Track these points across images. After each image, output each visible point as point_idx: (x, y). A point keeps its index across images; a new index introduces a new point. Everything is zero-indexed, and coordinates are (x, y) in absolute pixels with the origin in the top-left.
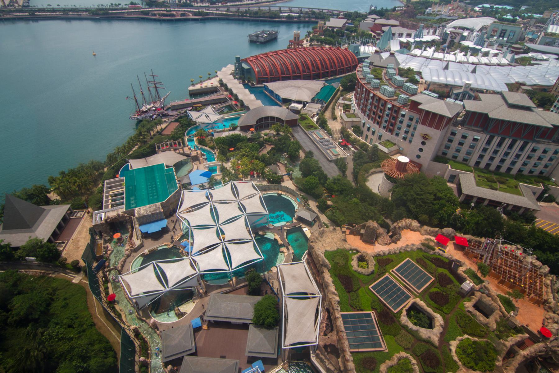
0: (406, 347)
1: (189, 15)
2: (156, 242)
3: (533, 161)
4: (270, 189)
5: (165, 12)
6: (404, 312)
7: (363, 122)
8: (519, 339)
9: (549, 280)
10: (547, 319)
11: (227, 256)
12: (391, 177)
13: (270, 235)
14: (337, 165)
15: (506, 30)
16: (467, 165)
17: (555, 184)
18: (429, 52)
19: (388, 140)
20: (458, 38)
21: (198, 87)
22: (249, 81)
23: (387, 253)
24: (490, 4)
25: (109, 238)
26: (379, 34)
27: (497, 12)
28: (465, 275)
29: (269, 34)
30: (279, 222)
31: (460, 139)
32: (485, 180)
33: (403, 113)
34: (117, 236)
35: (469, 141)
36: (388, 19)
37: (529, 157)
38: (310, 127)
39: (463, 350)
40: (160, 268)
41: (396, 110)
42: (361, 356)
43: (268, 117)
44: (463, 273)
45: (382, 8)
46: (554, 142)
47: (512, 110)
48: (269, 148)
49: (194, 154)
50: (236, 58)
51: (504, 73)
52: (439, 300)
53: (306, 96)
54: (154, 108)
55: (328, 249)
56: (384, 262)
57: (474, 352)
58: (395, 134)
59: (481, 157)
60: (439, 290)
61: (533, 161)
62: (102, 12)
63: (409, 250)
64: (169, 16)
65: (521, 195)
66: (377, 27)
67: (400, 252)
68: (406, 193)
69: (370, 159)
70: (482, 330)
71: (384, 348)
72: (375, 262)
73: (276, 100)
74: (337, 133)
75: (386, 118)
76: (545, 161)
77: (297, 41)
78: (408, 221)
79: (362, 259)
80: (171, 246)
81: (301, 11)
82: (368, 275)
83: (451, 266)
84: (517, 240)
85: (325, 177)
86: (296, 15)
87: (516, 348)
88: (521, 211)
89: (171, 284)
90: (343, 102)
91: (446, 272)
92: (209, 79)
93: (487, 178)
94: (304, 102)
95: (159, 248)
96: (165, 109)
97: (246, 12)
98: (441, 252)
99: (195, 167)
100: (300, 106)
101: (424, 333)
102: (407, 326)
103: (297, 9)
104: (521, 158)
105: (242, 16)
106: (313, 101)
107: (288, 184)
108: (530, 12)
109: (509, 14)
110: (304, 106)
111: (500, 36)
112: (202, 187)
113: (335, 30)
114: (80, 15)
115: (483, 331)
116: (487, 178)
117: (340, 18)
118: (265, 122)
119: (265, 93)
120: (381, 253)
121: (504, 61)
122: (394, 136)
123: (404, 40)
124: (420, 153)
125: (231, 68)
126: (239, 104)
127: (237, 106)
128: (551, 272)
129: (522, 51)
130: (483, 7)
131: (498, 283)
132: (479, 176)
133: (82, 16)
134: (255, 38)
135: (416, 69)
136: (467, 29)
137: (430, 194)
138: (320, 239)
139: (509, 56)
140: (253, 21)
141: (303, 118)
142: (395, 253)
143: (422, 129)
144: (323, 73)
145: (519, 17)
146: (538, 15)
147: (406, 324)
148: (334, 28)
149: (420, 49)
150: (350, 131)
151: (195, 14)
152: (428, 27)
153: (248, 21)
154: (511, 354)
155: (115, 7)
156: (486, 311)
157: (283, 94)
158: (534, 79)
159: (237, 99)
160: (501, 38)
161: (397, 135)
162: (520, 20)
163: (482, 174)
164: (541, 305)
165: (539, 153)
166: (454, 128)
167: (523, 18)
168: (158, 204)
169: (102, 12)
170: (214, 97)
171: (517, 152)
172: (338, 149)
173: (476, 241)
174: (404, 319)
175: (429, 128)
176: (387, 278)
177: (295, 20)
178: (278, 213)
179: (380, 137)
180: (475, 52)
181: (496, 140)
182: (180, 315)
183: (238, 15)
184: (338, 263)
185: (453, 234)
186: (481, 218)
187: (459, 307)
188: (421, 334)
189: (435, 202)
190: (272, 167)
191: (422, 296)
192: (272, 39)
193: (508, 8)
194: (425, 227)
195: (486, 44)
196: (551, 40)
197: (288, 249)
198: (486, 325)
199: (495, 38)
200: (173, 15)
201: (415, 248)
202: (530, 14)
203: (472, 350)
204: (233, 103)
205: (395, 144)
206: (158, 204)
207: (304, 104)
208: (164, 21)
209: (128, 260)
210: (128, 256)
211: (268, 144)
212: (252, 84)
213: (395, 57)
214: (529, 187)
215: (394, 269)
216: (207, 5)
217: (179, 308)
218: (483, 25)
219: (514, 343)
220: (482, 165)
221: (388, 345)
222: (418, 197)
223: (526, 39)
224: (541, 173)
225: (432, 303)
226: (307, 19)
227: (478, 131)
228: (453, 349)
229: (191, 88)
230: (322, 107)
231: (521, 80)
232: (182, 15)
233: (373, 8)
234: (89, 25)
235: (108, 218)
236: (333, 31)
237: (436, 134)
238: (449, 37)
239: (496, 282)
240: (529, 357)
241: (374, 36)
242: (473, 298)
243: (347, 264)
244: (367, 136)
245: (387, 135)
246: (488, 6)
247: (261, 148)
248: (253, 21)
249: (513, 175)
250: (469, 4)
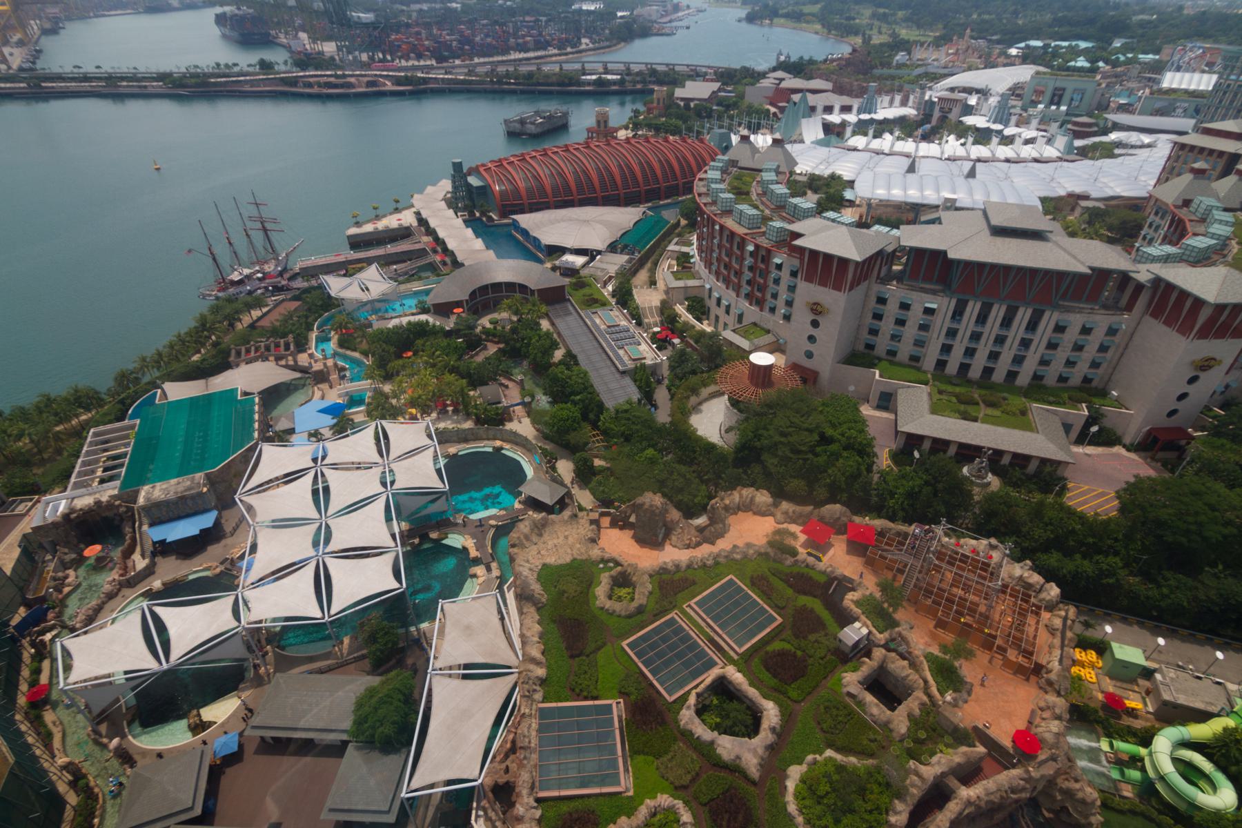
0: (677, 784)
1: (385, 85)
2: (187, 562)
3: (1062, 355)
4: (477, 438)
5: (332, 79)
6: (692, 700)
7: (708, 286)
8: (958, 759)
9: (1060, 616)
10: (1042, 709)
11: (323, 585)
12: (738, 402)
13: (455, 540)
14: (635, 381)
15: (1064, 89)
16: (919, 369)
17: (1119, 403)
18: (886, 142)
19: (755, 324)
20: (956, 110)
21: (368, 228)
22: (483, 213)
23: (684, 565)
25: (74, 556)
26: (782, 110)
27: (1056, 53)
28: (857, 611)
29: (550, 117)
30: (487, 508)
31: (897, 311)
32: (954, 399)
33: (777, 261)
34: (93, 551)
35: (915, 316)
36: (810, 78)
37: (1052, 346)
38: (594, 302)
39: (810, 788)
40: (156, 617)
41: (764, 256)
42: (565, 808)
44: (853, 607)
45: (801, 58)
46: (1105, 307)
47: (1000, 241)
48: (492, 349)
49: (317, 367)
50: (454, 164)
51: (1043, 176)
52: (783, 669)
53: (597, 239)
54: (260, 275)
55: (551, 560)
56: (672, 585)
57: (834, 790)
59: (946, 349)
60: (787, 646)
61: (1062, 355)
62: (193, 81)
63: (738, 557)
65: (1031, 430)
66: (782, 95)
67: (717, 564)
68: (761, 432)
69: (701, 363)
70: (872, 737)
71: (625, 784)
72: (650, 587)
73: (534, 251)
74: (652, 313)
75: (747, 275)
76: (1090, 352)
77: (602, 128)
78: (747, 492)
79: (623, 580)
80: (218, 570)
81: (628, 69)
82: (630, 616)
83: (831, 590)
84: (1003, 529)
85: (601, 407)
86: (615, 77)
87: (953, 782)
88: (1032, 467)
89: (177, 652)
90: (677, 248)
91: (815, 604)
92: (397, 210)
93: (957, 396)
94: (592, 251)
95: (191, 577)
96: (287, 276)
97: (508, 75)
98: (811, 560)
99: (318, 394)
100: (579, 260)
101: (727, 746)
102: (691, 733)
103: (622, 67)
104: (1033, 348)
105: (500, 82)
106: (612, 248)
107: (523, 426)
108: (1132, 50)
109: (1082, 58)
110: (593, 258)
111: (1052, 103)
112: (315, 435)
113: (692, 105)
114: (145, 87)
115: (875, 740)
116: (957, 396)
117: (707, 80)
118: (487, 296)
119: (514, 237)
120: (670, 566)
121: (1050, 152)
122: (766, 314)
123: (835, 118)
124: (811, 347)
125: (446, 185)
126: (448, 260)
127: (445, 264)
128: (1066, 597)
129: (1096, 129)
130: (1028, 47)
131: (935, 627)
132: (940, 392)
133: (150, 90)
134: (518, 126)
135: (847, 176)
136: (978, 91)
137: (810, 431)
138: (535, 538)
139: (1061, 141)
140: (523, 92)
141: (581, 285)
142: (705, 565)
143: (808, 291)
144: (647, 191)
145: (1106, 63)
146: (1151, 56)
147: (689, 727)
148: (692, 100)
149: (865, 134)
150: (680, 309)
151: (398, 81)
152: (891, 91)
153: (513, 92)
154: (937, 796)
155: (223, 70)
156: (886, 689)
157: (548, 237)
158: (1112, 185)
159: (446, 250)
160: (1054, 107)
161: (773, 310)
162: (1108, 67)
163: (950, 388)
164: (1033, 678)
165: (1072, 335)
166: (881, 288)
167: (1115, 64)
168: (199, 476)
169: (193, 81)
170: (404, 246)
172: (644, 347)
173: (898, 534)
174: (687, 716)
175: (822, 289)
176: (672, 620)
178: (487, 490)
179: (740, 318)
180: (983, 136)
181: (973, 309)
182: (199, 727)
183: (492, 81)
184: (564, 592)
185: (844, 519)
186: (918, 482)
187: (829, 685)
188: (719, 751)
189: (818, 449)
190: (489, 390)
191: (744, 663)
192: (558, 127)
193: (1083, 45)
194: (785, 505)
195: (1014, 119)
196: (1166, 104)
197: (489, 569)
198: (886, 725)
199: (1041, 106)
200: (350, 85)
201: (751, 552)
202: (1130, 55)
203: (828, 788)
204: (438, 258)
205: (768, 332)
206: (199, 476)
207: (591, 254)
208: (330, 97)
209: (108, 606)
210: (111, 596)
211: (492, 341)
212: (490, 219)
213: (750, 143)
214: (1055, 413)
215: (692, 603)
216: (428, 63)
217: (202, 711)
218: (1015, 80)
219: (944, 768)
220: (952, 368)
221: (635, 778)
222: (782, 439)
223: (1112, 104)
224: (1087, 380)
225: (765, 676)
226: (639, 86)
227: (934, 292)
228: (791, 785)
229: (353, 231)
230: (629, 261)
231: (1078, 189)
232: (369, 84)
233: (782, 58)
234: (165, 112)
235: (72, 511)
236: (687, 107)
237: (835, 300)
238: (937, 108)
239: (932, 624)
240: (983, 804)
241: (775, 114)
242: (864, 663)
243: (587, 594)
244: (717, 317)
245: (752, 312)
246: (1038, 43)
247: (470, 354)
249: (1022, 388)
250: (998, 42)
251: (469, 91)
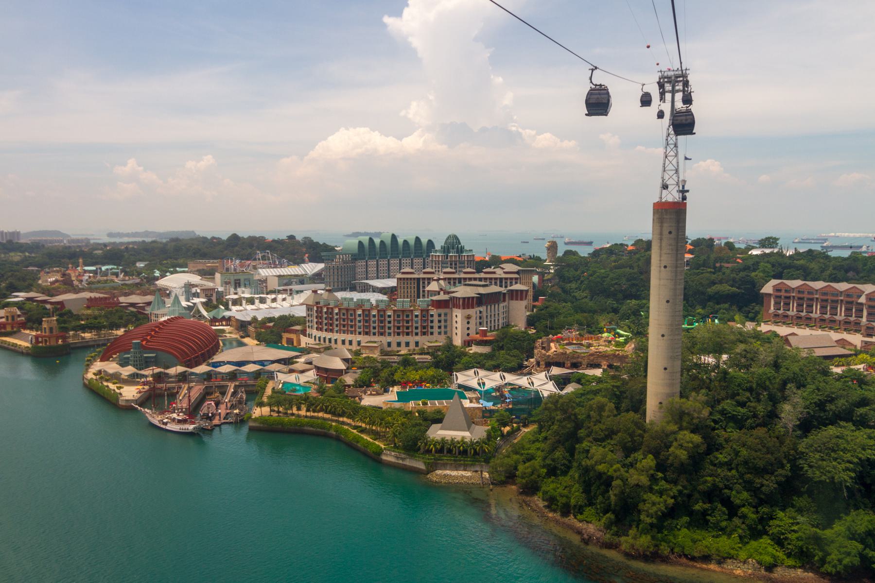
161: (432, 334)
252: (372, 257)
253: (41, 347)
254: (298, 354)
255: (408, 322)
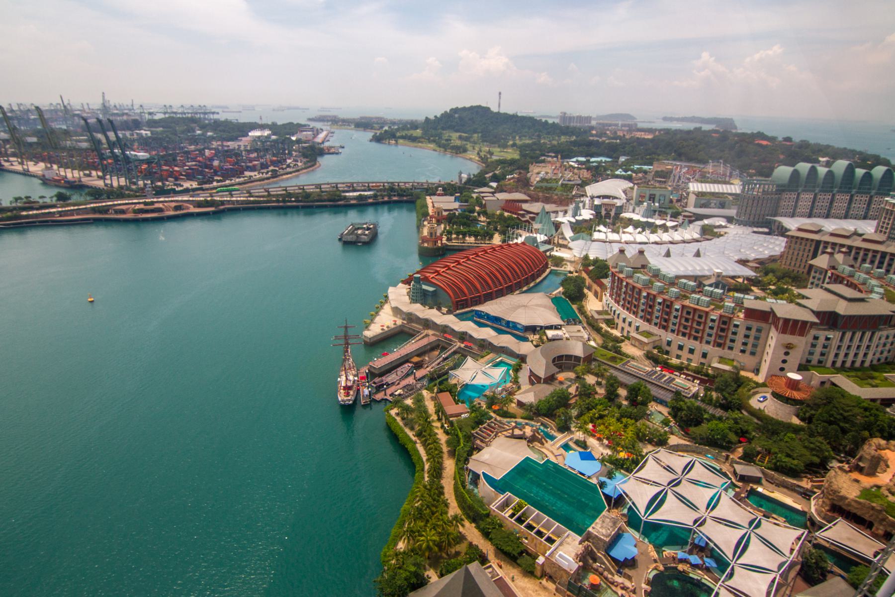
1: (188, 208)
5: (142, 206)
24: (585, 157)
43: (571, 356)
58: (726, 348)
59: (837, 355)
64: (153, 211)
140: (303, 207)
151: (199, 204)
161: (731, 348)
171: (848, 343)
177: (370, 201)
200: (160, 210)
226: (386, 199)
232: (177, 208)
237: (801, 343)
248: (303, 207)
251: (245, 209)
252: (824, 190)
253: (427, 248)
254: (528, 198)
255: (699, 323)
